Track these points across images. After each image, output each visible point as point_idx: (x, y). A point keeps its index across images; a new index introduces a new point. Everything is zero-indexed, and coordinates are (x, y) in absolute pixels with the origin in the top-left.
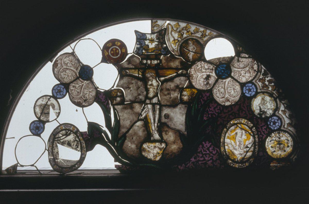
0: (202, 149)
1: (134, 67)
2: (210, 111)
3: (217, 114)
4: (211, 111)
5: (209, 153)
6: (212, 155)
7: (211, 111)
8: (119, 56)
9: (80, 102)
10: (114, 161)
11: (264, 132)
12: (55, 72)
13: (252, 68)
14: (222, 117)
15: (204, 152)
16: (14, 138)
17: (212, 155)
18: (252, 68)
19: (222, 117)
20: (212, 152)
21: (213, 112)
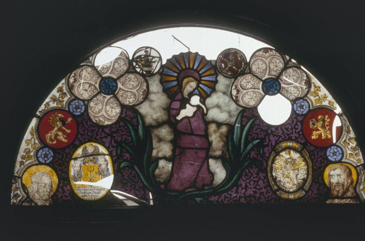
0: (87, 119)
1: (186, 191)
2: (317, 152)
3: (293, 130)
4: (318, 154)
5: (87, 128)
6: (86, 132)
7: (318, 154)
8: (242, 69)
9: (266, 53)
10: (168, 58)
11: (269, 196)
12: (257, 53)
13: (76, 80)
14: (259, 197)
15: (86, 122)
16: (172, 36)
17: (86, 132)
18: (76, 80)
19: (259, 197)
20: (90, 131)
21: (317, 155)
